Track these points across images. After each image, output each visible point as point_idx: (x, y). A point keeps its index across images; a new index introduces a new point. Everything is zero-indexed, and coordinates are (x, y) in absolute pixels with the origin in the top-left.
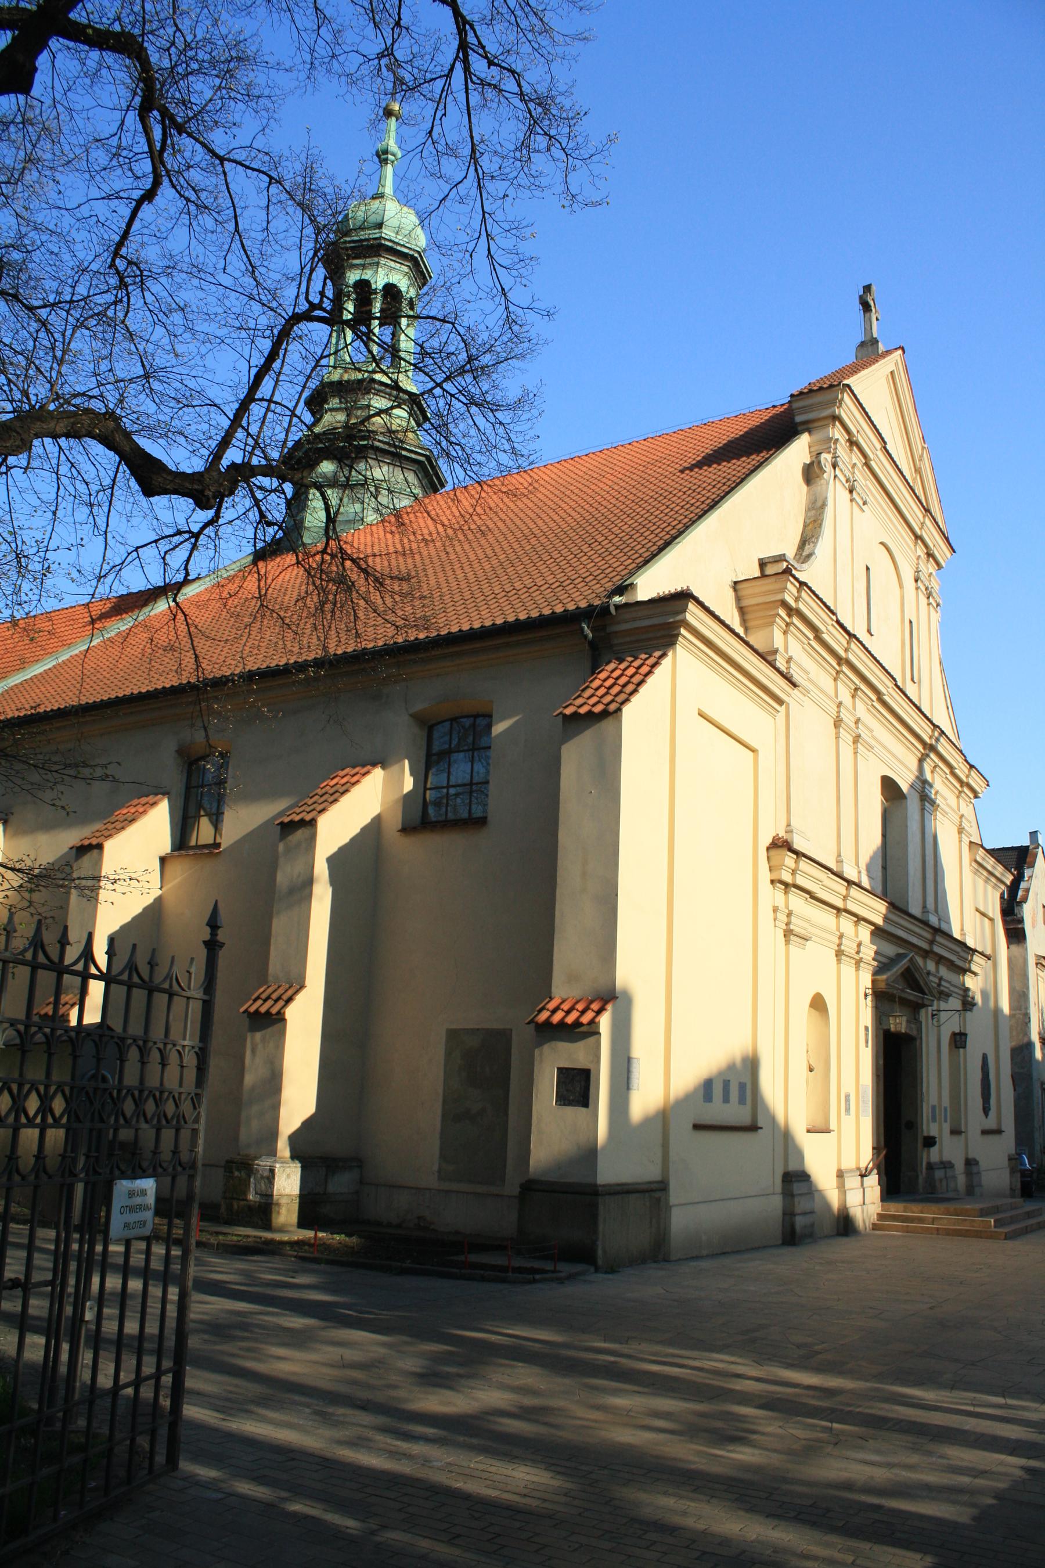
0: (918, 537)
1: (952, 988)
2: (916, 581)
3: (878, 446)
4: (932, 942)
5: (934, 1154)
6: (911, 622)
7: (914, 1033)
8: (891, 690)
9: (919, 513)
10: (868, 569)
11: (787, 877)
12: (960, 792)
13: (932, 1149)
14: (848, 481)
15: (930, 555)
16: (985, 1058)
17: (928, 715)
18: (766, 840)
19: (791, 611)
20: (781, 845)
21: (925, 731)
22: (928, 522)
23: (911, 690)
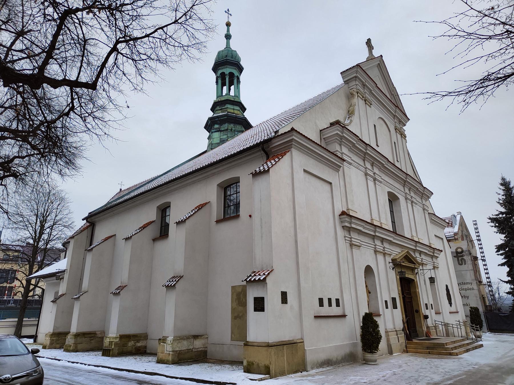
0: (394, 116)
1: (361, 243)
2: (396, 130)
3: (374, 86)
4: (433, 253)
5: (429, 320)
6: (395, 143)
7: (414, 279)
8: (387, 163)
9: (394, 108)
10: (375, 126)
11: (347, 224)
12: (422, 197)
13: (428, 320)
14: (363, 97)
15: (364, 85)
16: (447, 286)
17: (406, 172)
18: (338, 212)
19: (342, 137)
20: (343, 213)
21: (403, 177)
22: (398, 110)
23: (397, 164)
